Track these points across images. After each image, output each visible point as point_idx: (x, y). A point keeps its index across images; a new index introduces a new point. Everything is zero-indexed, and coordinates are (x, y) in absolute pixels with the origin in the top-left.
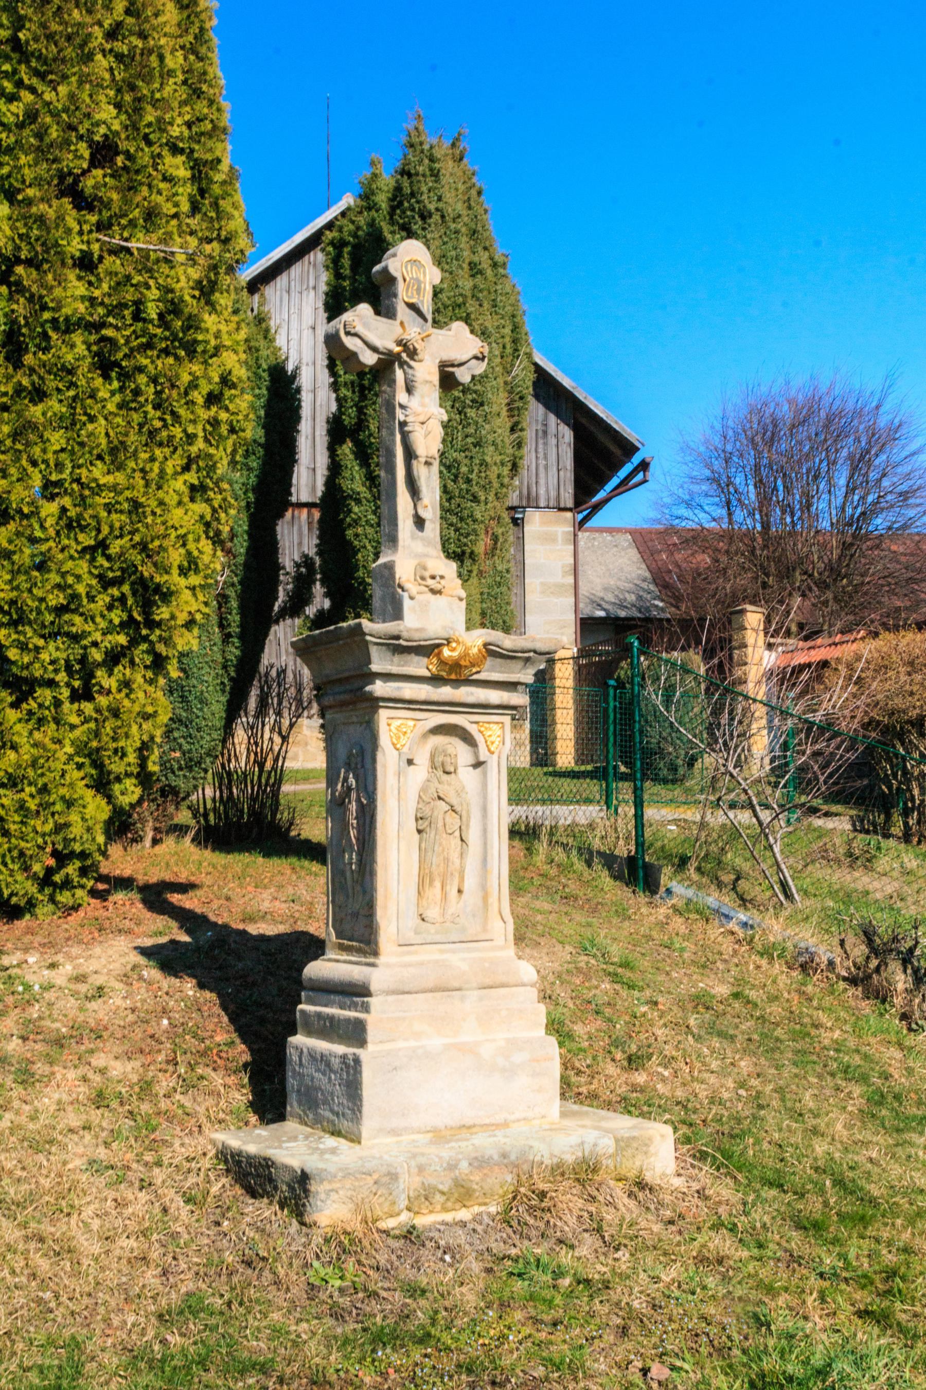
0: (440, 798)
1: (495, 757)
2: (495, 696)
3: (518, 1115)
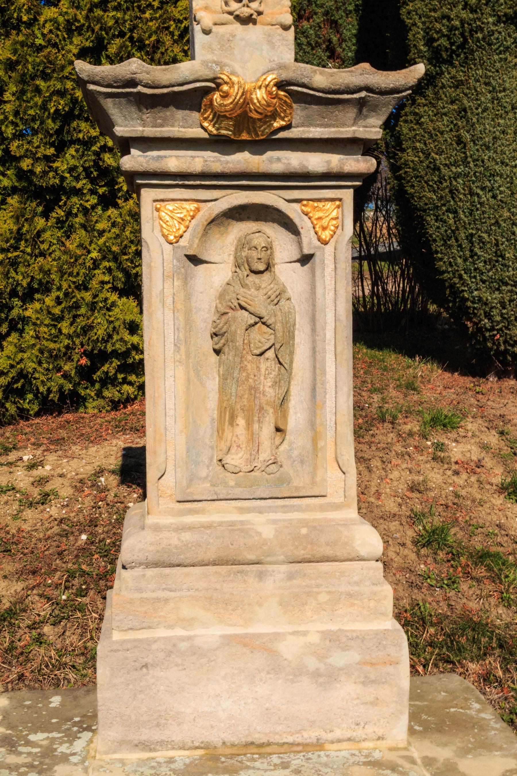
0: (242, 308)
1: (329, 249)
2: (316, 162)
3: (338, 734)
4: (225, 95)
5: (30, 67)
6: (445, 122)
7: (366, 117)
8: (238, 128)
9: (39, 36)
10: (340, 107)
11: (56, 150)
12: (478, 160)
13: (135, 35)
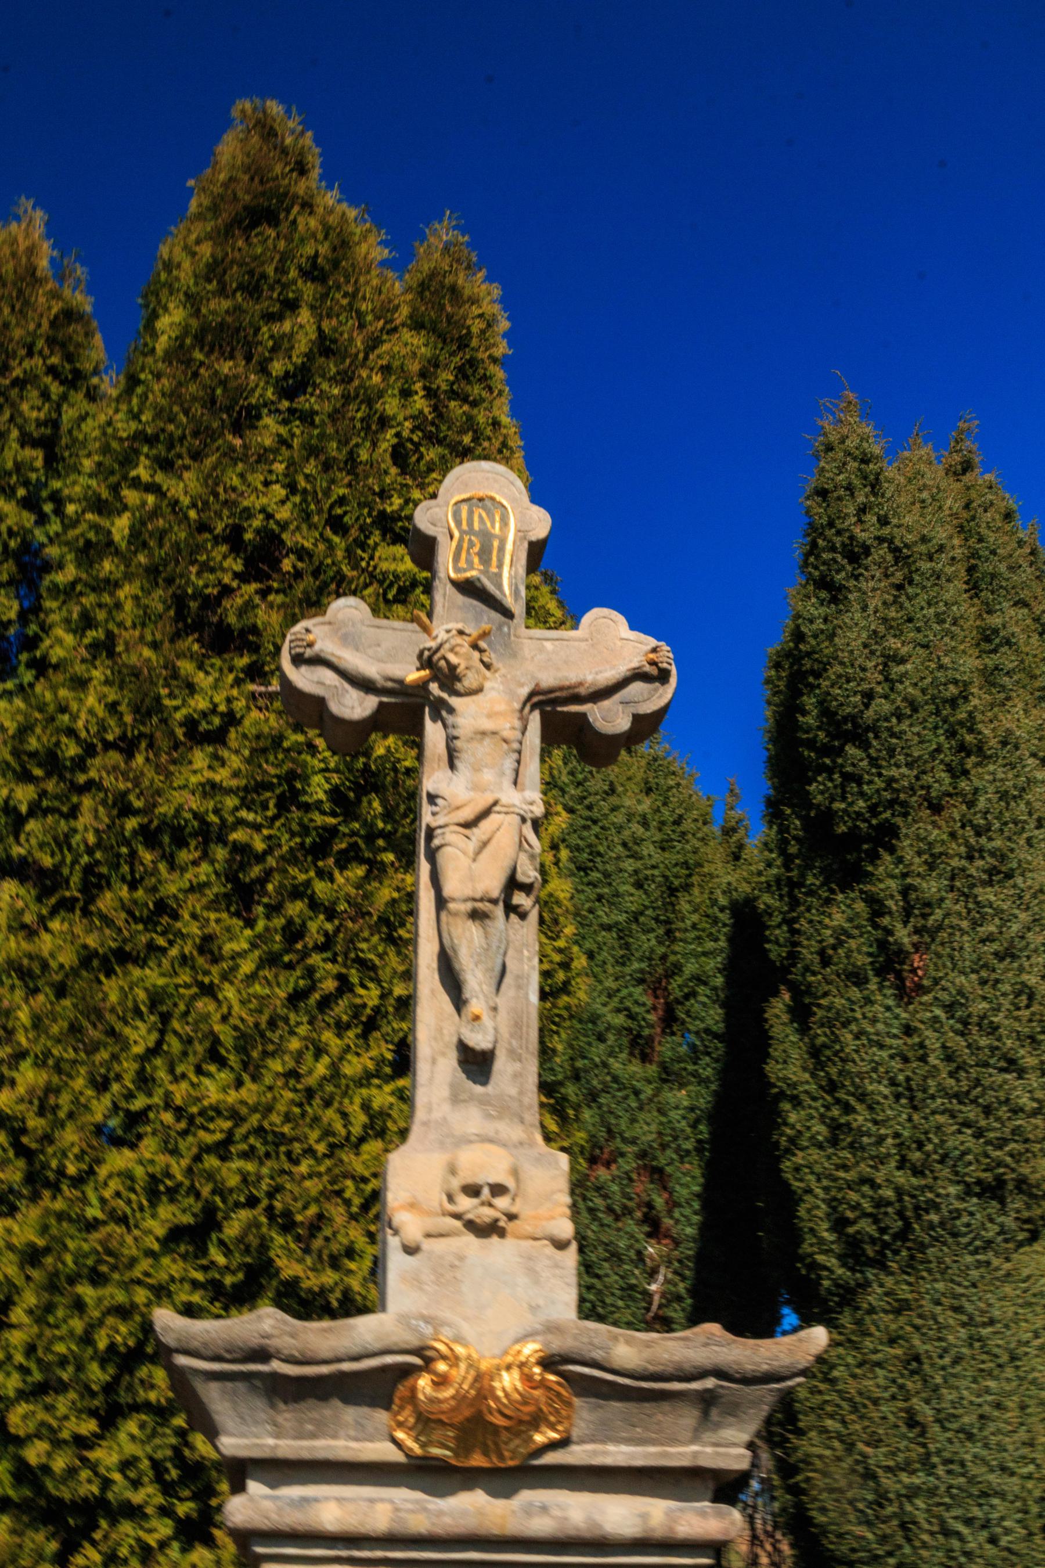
4: (442, 1381)
5: (69, 1259)
6: (881, 1381)
7: (718, 1426)
8: (464, 1447)
9: (94, 1201)
10: (666, 1406)
11: (100, 1426)
12: (951, 1462)
13: (278, 1205)
